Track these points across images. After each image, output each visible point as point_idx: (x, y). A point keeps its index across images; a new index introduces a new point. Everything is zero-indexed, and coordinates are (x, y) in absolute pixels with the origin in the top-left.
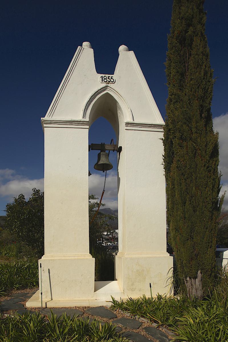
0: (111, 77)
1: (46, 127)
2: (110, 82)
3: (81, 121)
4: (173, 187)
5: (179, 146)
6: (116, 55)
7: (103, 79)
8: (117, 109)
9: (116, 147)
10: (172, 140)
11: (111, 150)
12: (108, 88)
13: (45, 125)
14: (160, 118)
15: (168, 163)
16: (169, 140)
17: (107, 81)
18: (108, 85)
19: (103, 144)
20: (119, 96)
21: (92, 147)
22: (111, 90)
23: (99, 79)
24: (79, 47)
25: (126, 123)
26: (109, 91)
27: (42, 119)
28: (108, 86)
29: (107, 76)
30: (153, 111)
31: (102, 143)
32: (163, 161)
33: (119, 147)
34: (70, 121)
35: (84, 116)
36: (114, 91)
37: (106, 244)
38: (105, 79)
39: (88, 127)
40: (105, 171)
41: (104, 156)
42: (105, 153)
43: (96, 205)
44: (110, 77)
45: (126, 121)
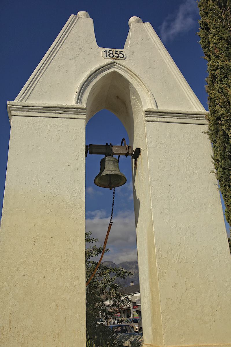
6: (126, 29)
7: (108, 54)
9: (130, 150)
12: (116, 65)
13: (13, 113)
17: (113, 57)
19: (109, 144)
20: (132, 76)
21: (90, 149)
23: (102, 54)
24: (72, 15)
27: (8, 102)
31: (107, 144)
32: (213, 166)
33: (134, 149)
34: (56, 107)
35: (79, 99)
37: (109, 321)
38: (110, 54)
39: (85, 117)
40: (113, 188)
41: (111, 163)
43: (94, 251)
44: (117, 51)
45: (145, 109)
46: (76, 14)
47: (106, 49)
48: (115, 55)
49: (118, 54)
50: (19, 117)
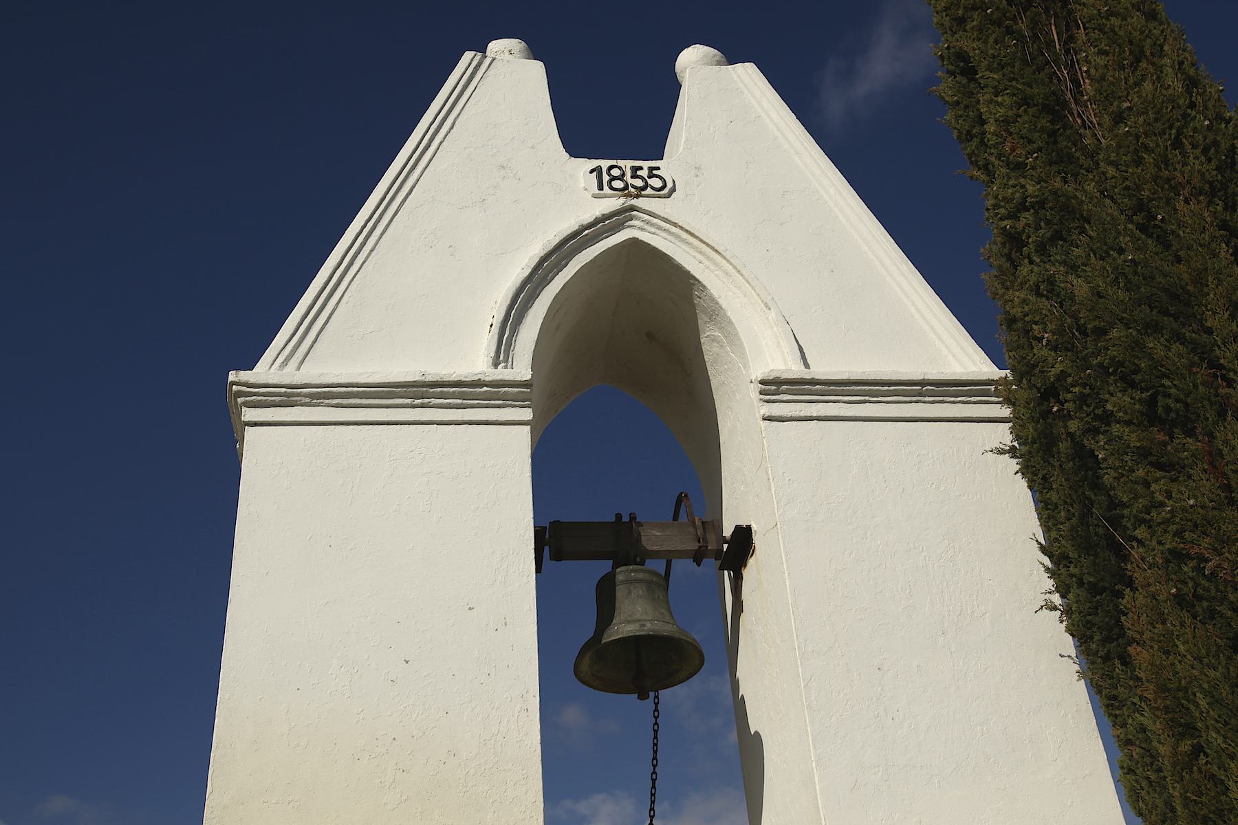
0: (651, 169)
1: (256, 424)
2: (644, 188)
3: (479, 384)
4: (1185, 746)
5: (1152, 464)
6: (671, 88)
7: (606, 178)
8: (700, 322)
10: (1089, 443)
11: (682, 554)
12: (637, 218)
13: (249, 414)
14: (962, 349)
15: (1094, 590)
16: (1064, 446)
17: (626, 188)
18: (635, 202)
19: (626, 519)
20: (700, 252)
22: (653, 225)
23: (582, 180)
24: (468, 55)
25: (762, 382)
26: (643, 229)
27: (232, 376)
28: (633, 208)
29: (627, 165)
30: (917, 316)
31: (619, 516)
32: (1049, 584)
35: (503, 351)
36: (673, 229)
38: (614, 178)
39: (527, 414)
40: (652, 694)
41: (639, 591)
42: (642, 571)
44: (641, 168)
45: (760, 372)
47: (595, 163)
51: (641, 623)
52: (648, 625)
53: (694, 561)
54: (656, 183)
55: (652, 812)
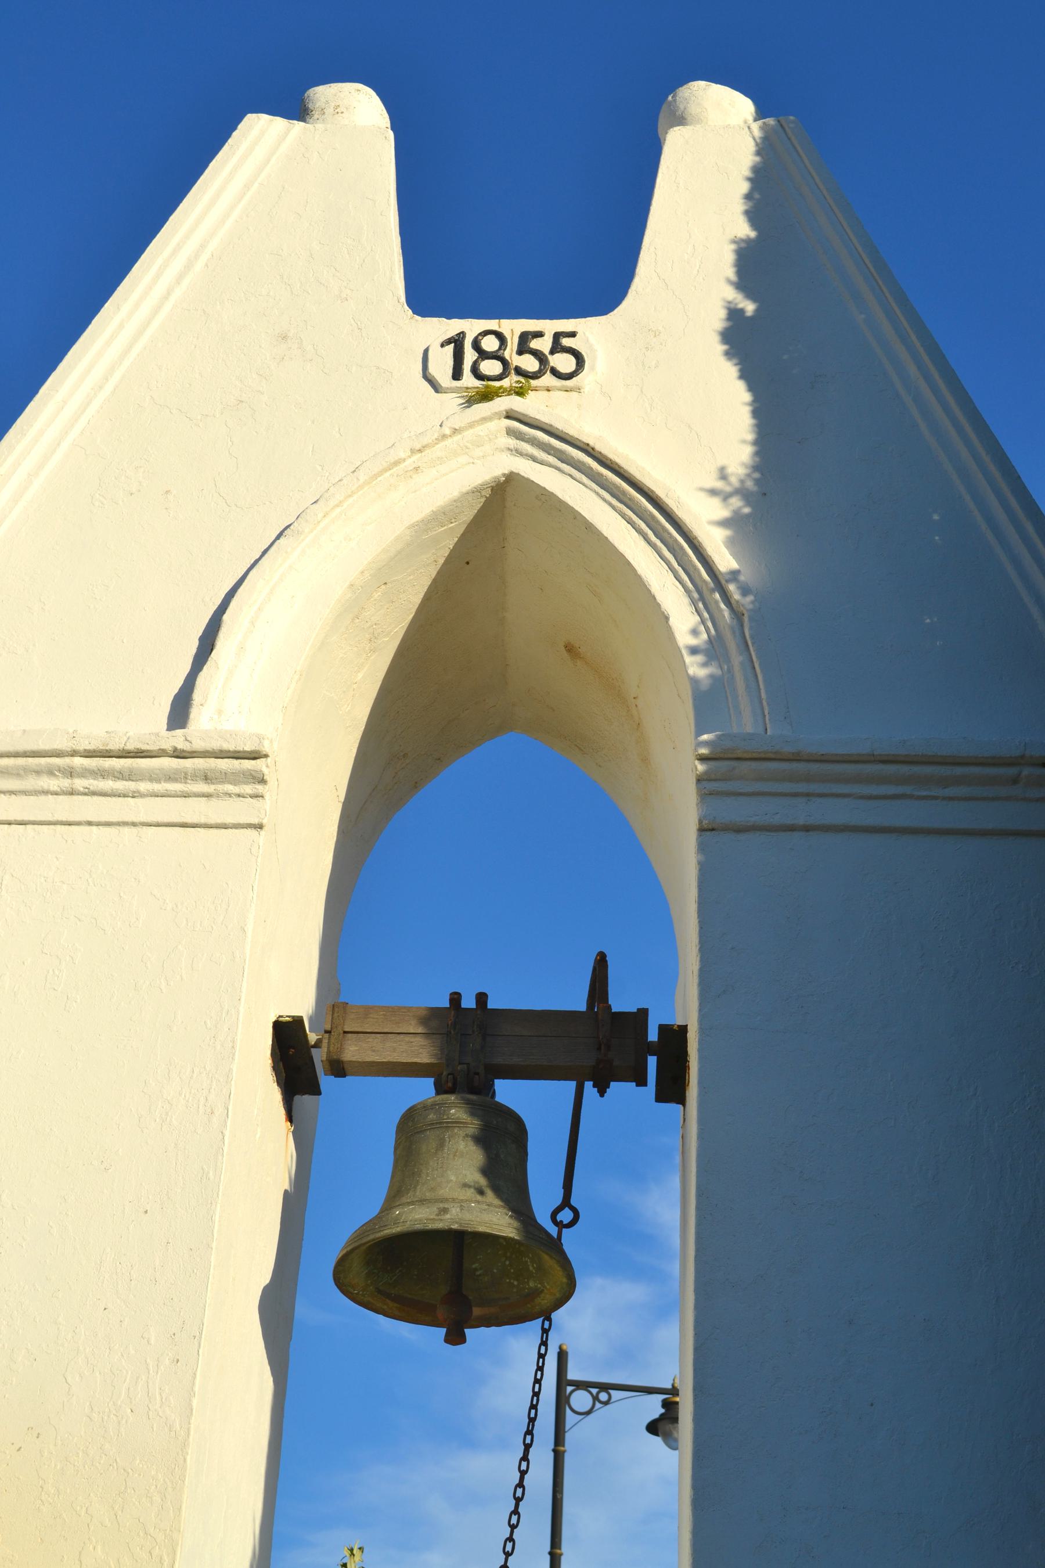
0: (557, 336)
7: (470, 356)
19: (469, 1002)
29: (513, 328)
31: (455, 998)
44: (539, 335)
46: (749, 179)
47: (454, 326)
48: (517, 361)
49: (537, 354)
50: (73, 827)
51: (441, 1205)
52: (454, 1211)
53: (594, 1086)
54: (564, 363)
55: (528, 1438)
